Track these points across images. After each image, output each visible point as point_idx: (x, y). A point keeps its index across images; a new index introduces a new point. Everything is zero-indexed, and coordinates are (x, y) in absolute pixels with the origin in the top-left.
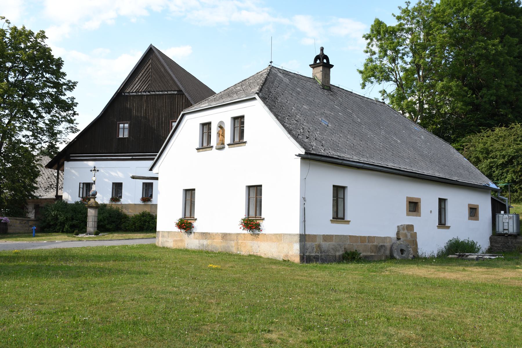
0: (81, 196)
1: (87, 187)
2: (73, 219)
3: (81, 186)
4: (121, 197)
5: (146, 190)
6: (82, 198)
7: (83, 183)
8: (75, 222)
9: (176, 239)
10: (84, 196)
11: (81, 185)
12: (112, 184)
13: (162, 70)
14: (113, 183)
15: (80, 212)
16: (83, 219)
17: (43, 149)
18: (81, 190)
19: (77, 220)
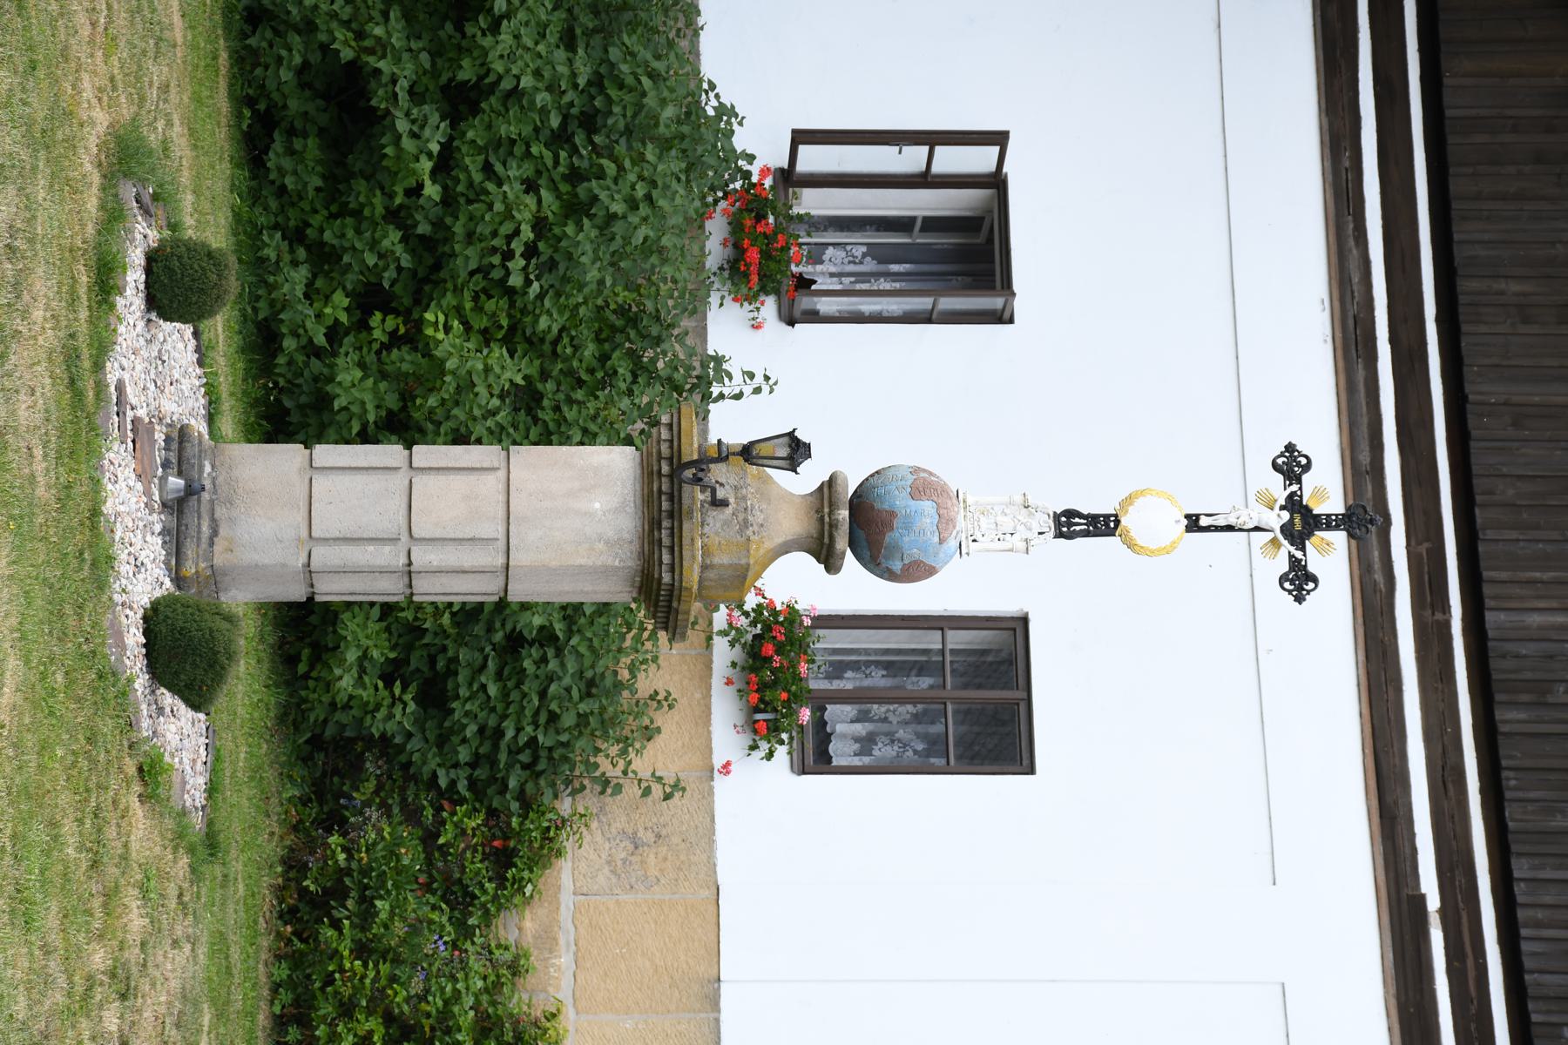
0: (813, 159)
1: (933, 224)
2: (461, 102)
3: (950, 160)
4: (816, 758)
5: (895, 664)
6: (788, 178)
7: (996, 182)
8: (416, 136)
9: (715, 248)
10: (812, 202)
11: (979, 160)
12: (1005, 606)
13: (1356, 280)
14: (1020, 625)
15: (576, 209)
16: (467, 258)
17: (574, 111)
18: (911, 159)
19: (445, 164)
